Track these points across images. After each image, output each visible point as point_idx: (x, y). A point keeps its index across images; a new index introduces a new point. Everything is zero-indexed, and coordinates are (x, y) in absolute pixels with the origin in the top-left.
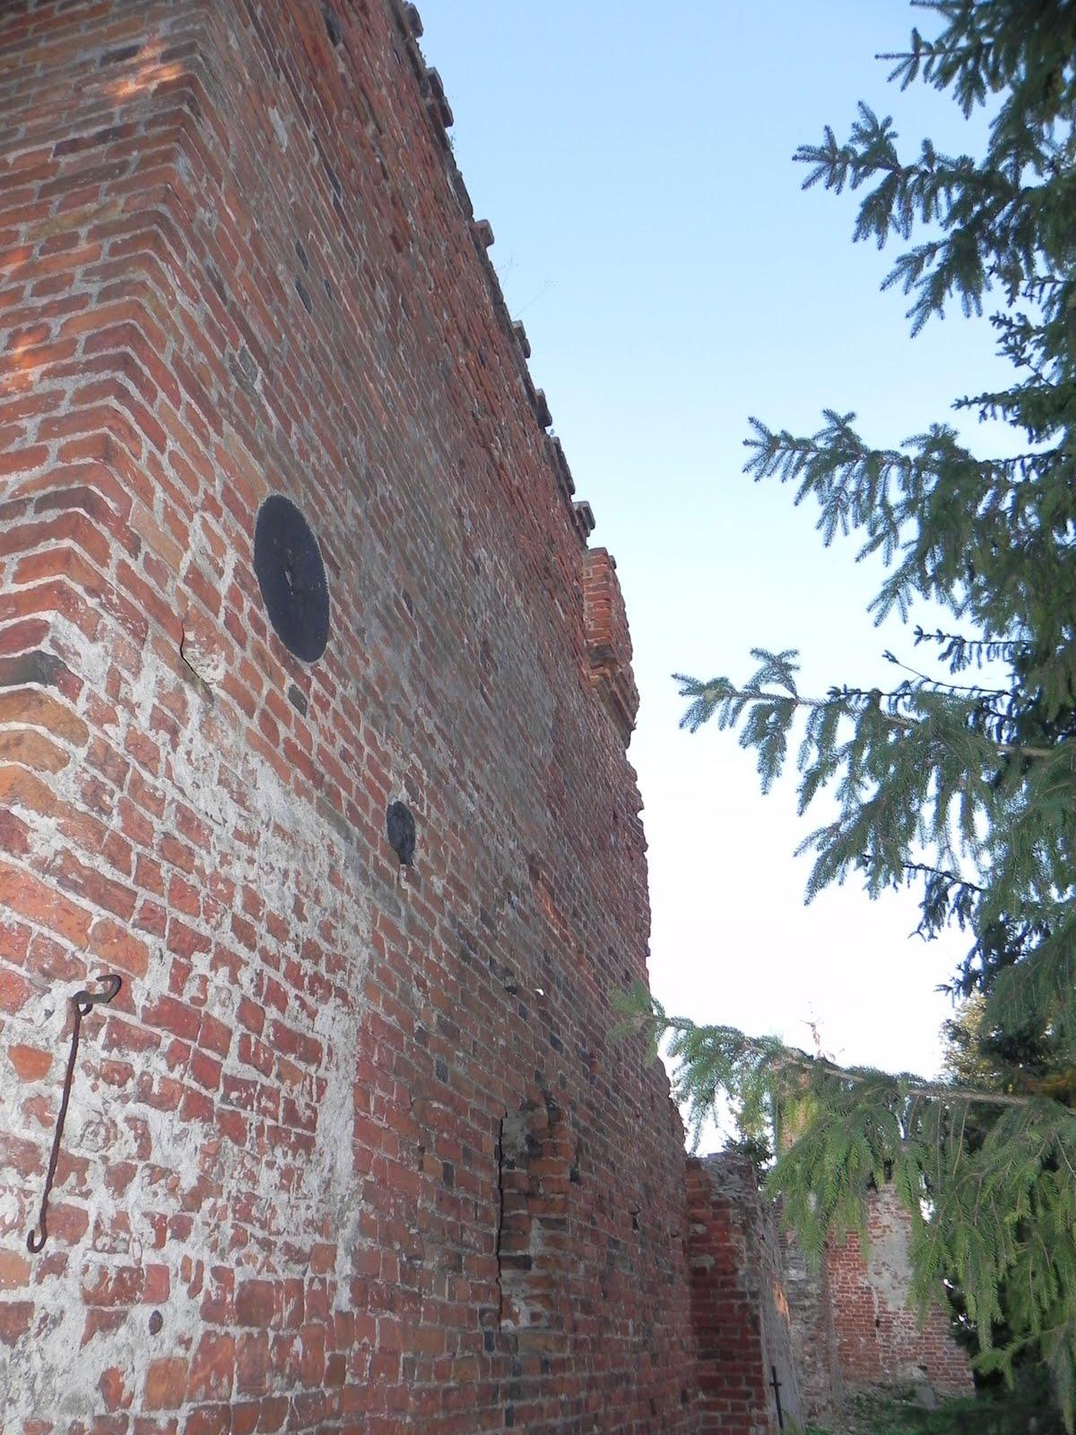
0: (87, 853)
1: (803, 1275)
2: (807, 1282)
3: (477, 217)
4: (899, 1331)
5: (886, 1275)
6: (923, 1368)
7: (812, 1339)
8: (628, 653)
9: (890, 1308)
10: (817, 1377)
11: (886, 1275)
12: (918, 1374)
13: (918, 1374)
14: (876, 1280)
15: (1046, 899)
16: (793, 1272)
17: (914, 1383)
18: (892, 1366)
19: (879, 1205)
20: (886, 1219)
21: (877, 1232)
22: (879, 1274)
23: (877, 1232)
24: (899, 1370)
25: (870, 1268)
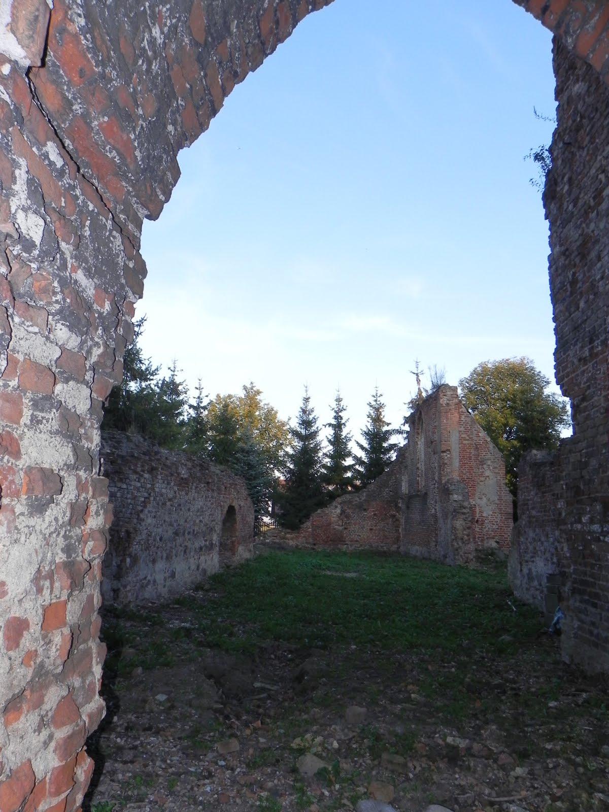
0: (41, 287)
1: (460, 498)
2: (463, 501)
3: (557, 103)
4: (488, 525)
5: (485, 499)
6: (497, 542)
7: (469, 528)
8: (552, 259)
9: (484, 515)
10: (469, 546)
11: (485, 499)
12: (494, 545)
13: (494, 545)
14: (478, 501)
15: (84, 30)
16: (455, 496)
17: (492, 549)
18: (482, 541)
19: (485, 466)
20: (488, 473)
21: (482, 479)
22: (480, 499)
23: (482, 479)
24: (485, 542)
25: (477, 495)
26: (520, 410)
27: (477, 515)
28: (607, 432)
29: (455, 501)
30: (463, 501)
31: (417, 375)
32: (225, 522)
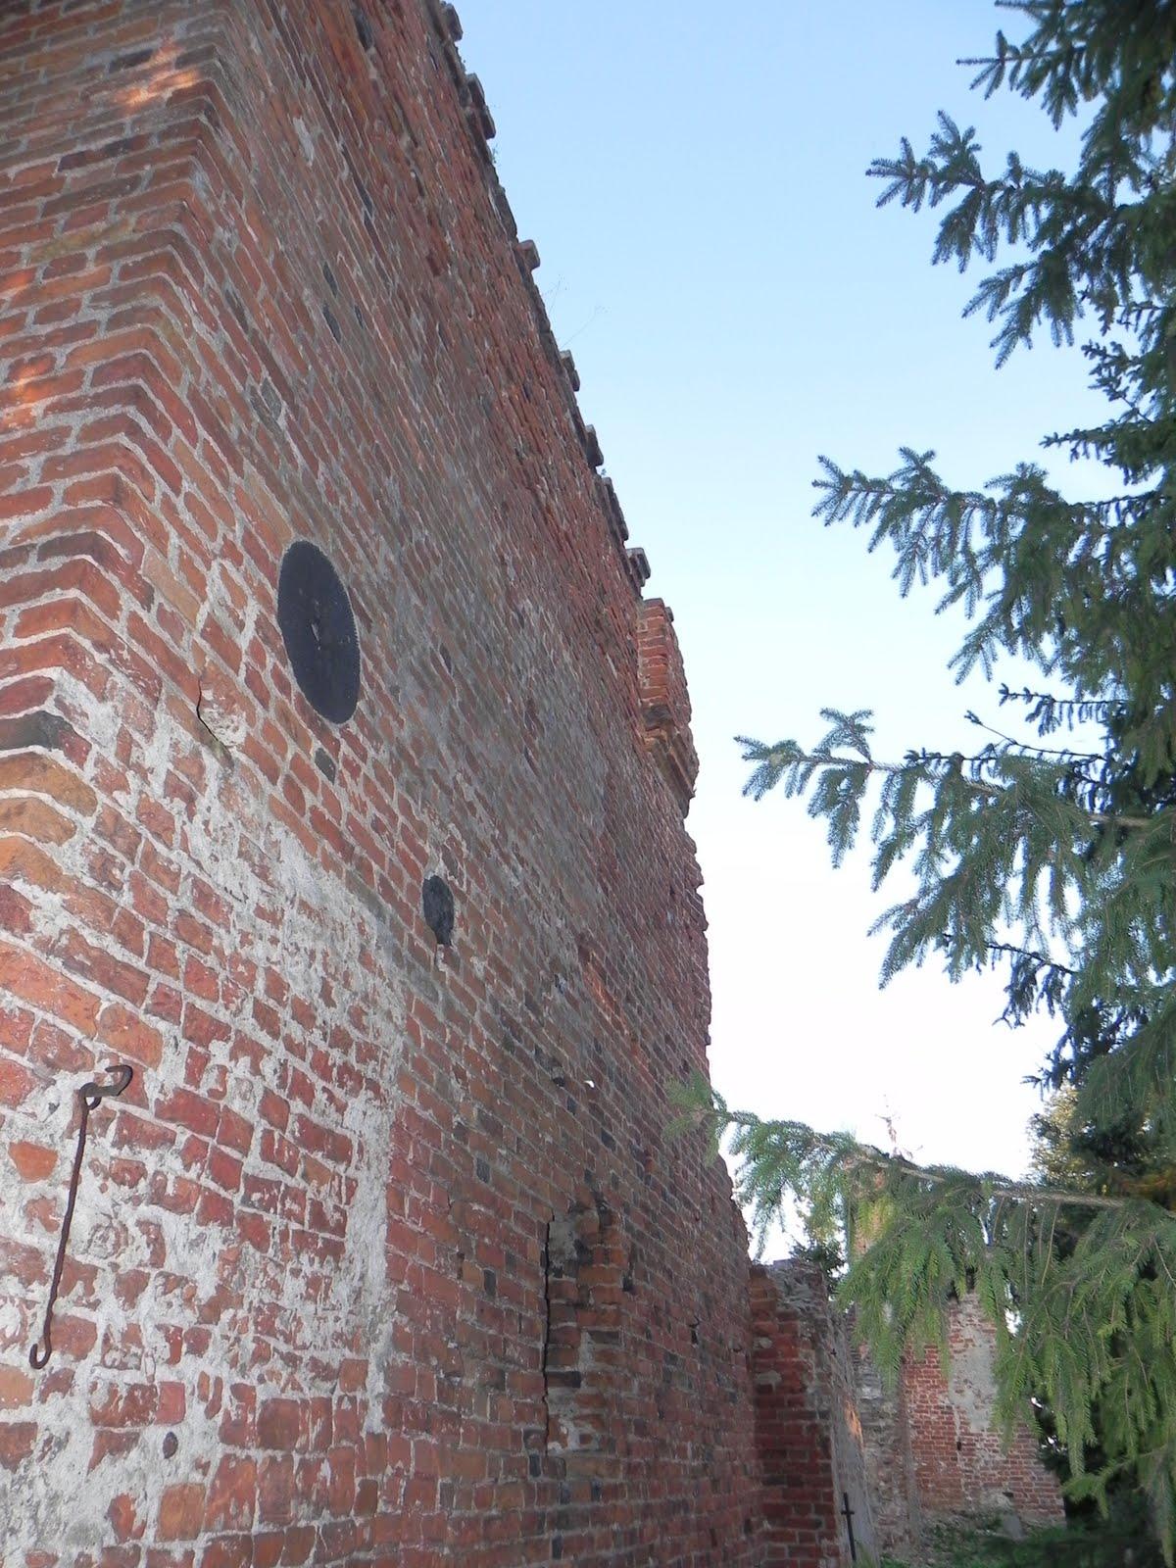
1: (877, 1393)
2: (882, 1401)
4: (983, 1455)
5: (969, 1393)
6: (1009, 1495)
7: (887, 1463)
9: (973, 1429)
10: (892, 1505)
11: (969, 1393)
12: (1003, 1501)
13: (1003, 1501)
14: (957, 1399)
16: (866, 1390)
17: (999, 1511)
18: (975, 1492)
19: (961, 1317)
20: (968, 1332)
21: (958, 1346)
22: (960, 1392)
23: (958, 1346)
25: (951, 1385)
26: (86, 805)
27: (958, 1431)
28: (1172, 677)
29: (865, 1401)
30: (882, 1401)
31: (888, 1121)
32: (1042, 1351)
